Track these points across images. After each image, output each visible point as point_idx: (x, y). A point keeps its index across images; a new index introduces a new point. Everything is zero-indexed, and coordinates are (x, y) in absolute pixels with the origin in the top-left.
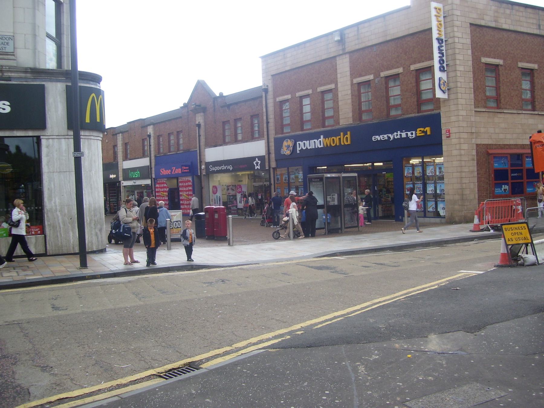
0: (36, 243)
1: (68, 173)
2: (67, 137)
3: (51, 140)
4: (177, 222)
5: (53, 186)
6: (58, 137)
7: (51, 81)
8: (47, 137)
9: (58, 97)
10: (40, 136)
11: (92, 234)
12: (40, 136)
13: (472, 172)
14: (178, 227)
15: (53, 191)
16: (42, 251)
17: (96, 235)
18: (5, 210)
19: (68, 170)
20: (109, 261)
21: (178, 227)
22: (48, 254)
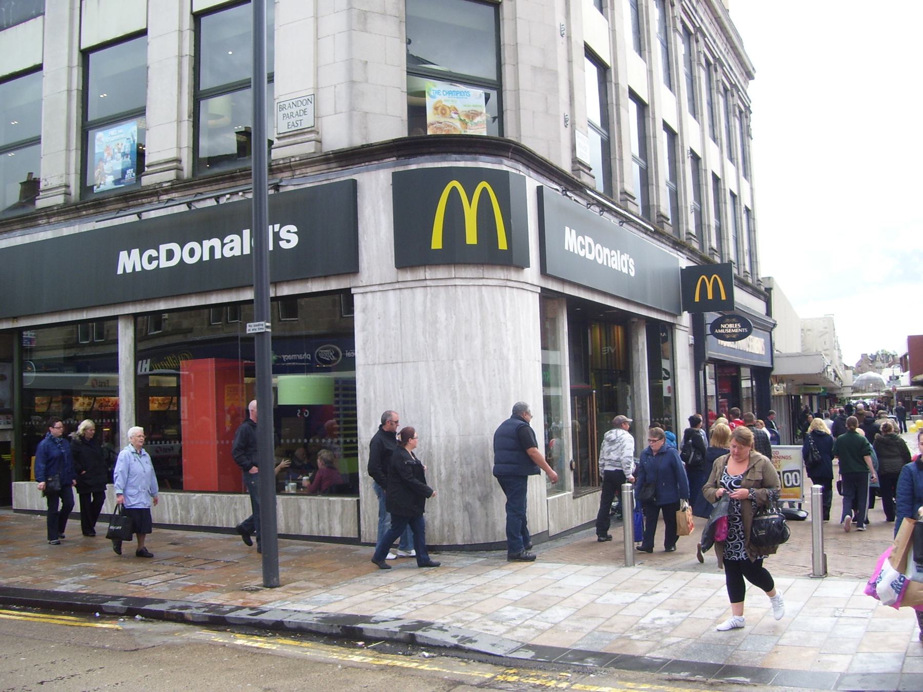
0: (342, 513)
1: (399, 365)
2: (397, 286)
3: (369, 295)
4: (791, 472)
5: (372, 396)
6: (381, 288)
7: (565, 173)
8: (362, 290)
9: (381, 202)
10: (350, 289)
11: (452, 505)
12: (350, 289)
13: (301, 530)
14: (793, 486)
15: (373, 406)
16: (353, 534)
17: (467, 507)
18: (306, 441)
19: (400, 360)
20: (227, 608)
21: (793, 486)
22: (363, 540)
